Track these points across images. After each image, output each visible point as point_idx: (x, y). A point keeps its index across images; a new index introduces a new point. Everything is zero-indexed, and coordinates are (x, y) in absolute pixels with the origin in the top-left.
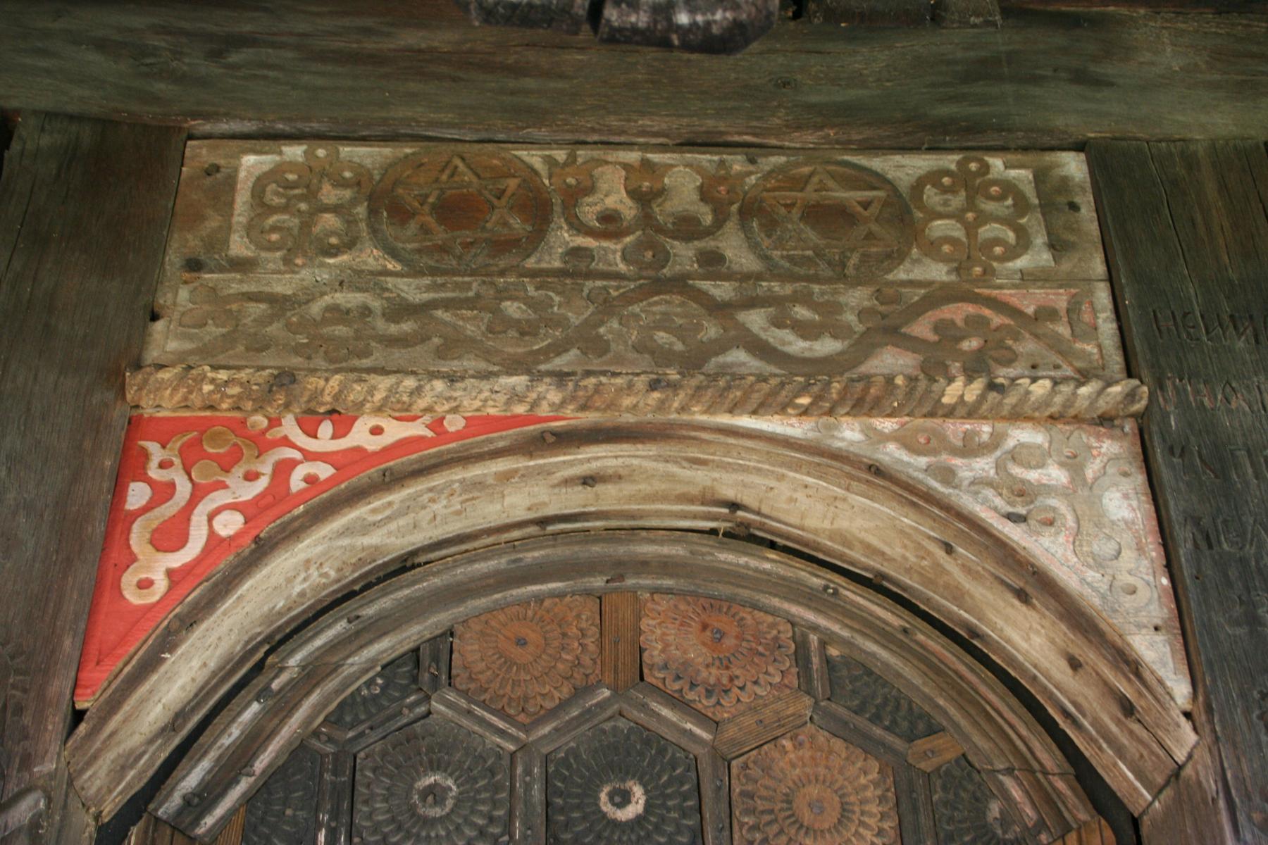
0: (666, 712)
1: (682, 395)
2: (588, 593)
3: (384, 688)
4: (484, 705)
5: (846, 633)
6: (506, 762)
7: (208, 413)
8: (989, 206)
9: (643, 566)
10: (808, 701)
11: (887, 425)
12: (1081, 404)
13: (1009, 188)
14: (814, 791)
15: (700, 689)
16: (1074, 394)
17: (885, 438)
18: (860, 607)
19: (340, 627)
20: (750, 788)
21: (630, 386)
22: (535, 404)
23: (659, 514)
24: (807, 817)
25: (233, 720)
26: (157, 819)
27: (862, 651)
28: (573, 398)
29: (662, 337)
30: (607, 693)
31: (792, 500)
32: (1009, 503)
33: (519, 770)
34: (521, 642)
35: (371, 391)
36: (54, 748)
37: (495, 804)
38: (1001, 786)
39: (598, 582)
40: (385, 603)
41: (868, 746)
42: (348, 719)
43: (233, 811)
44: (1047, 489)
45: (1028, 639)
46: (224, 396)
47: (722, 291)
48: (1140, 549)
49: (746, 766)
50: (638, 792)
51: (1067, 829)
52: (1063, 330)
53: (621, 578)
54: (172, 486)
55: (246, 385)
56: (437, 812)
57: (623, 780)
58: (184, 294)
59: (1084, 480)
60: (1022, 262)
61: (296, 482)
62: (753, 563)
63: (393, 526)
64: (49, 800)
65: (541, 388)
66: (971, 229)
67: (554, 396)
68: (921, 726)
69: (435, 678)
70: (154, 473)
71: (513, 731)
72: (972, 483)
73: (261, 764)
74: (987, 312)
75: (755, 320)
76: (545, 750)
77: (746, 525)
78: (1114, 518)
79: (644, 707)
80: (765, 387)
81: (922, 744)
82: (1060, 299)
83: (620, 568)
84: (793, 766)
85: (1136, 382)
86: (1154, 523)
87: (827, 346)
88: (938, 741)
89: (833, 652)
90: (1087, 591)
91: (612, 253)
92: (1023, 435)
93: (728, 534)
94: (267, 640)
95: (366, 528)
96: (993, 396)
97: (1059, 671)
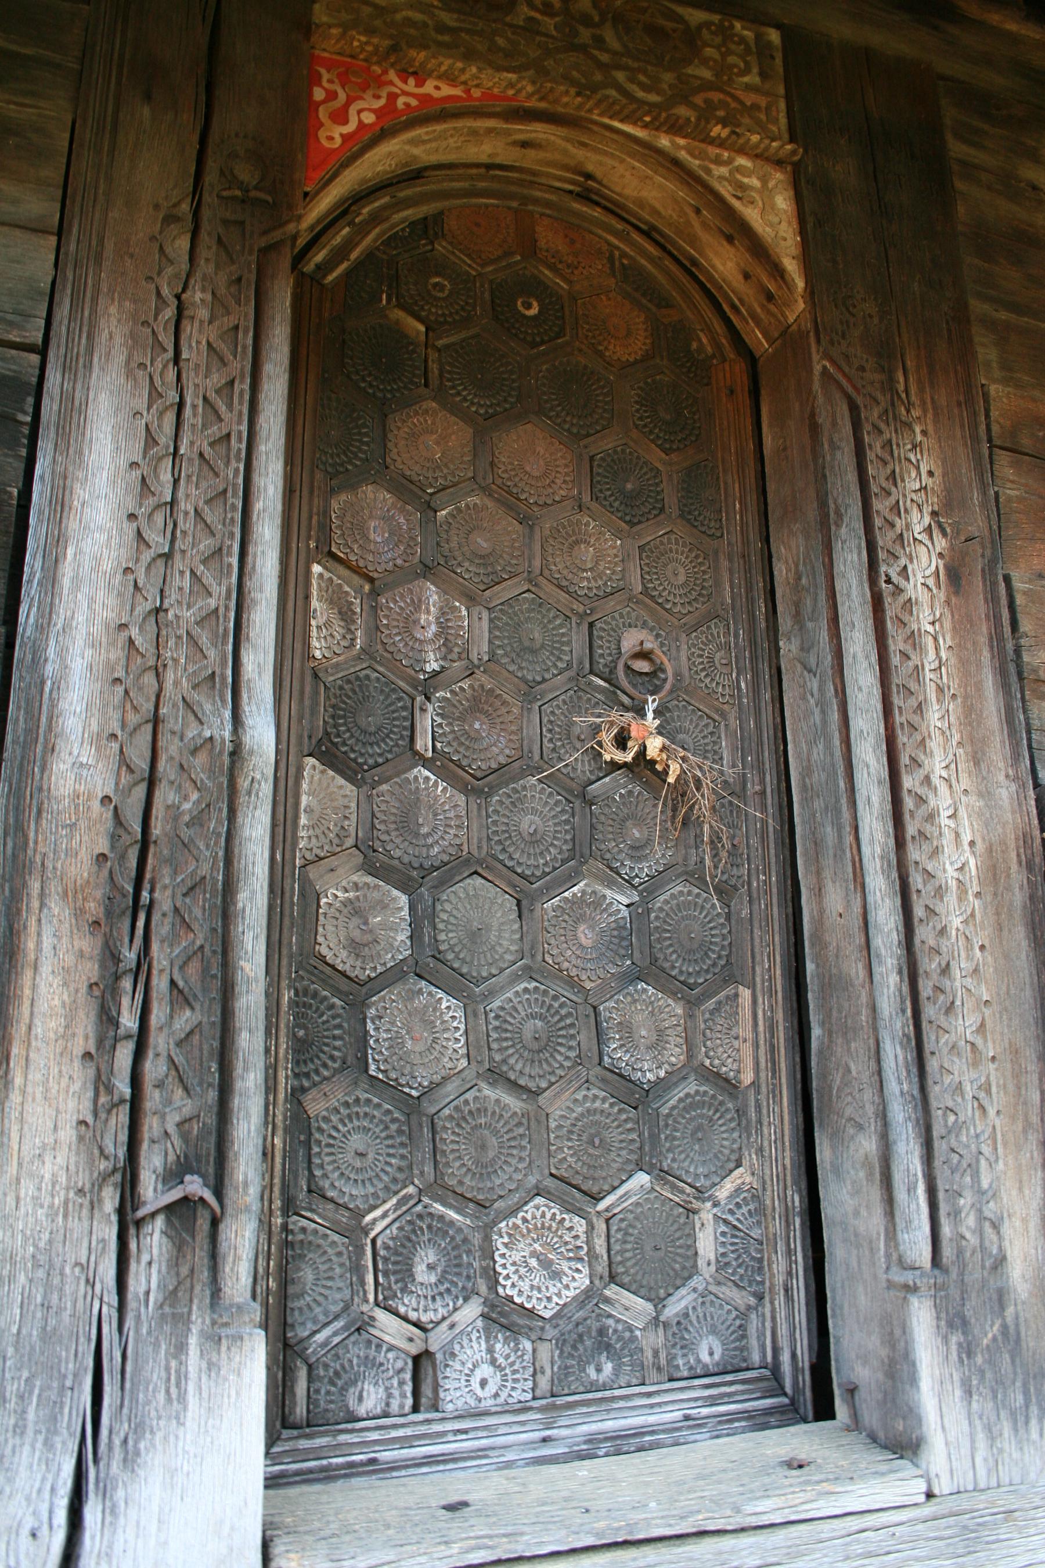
0: (547, 272)
2: (509, 208)
4: (460, 251)
8: (733, 47)
9: (536, 201)
11: (682, 142)
13: (743, 40)
17: (680, 148)
19: (387, 199)
22: (519, 91)
23: (548, 175)
26: (303, 274)
31: (622, 176)
34: (477, 225)
35: (440, 64)
39: (514, 204)
40: (408, 192)
44: (752, 188)
45: (724, 265)
47: (605, 58)
48: (789, 223)
50: (535, 304)
51: (724, 360)
52: (763, 117)
56: (441, 295)
60: (746, 79)
62: (589, 211)
65: (524, 83)
66: (724, 56)
69: (436, 234)
70: (325, 84)
73: (354, 256)
74: (729, 100)
75: (620, 76)
77: (589, 190)
79: (536, 268)
82: (763, 102)
83: (525, 200)
87: (653, 98)
89: (625, 262)
91: (549, 24)
92: (742, 161)
93: (578, 195)
96: (734, 137)
97: (736, 280)
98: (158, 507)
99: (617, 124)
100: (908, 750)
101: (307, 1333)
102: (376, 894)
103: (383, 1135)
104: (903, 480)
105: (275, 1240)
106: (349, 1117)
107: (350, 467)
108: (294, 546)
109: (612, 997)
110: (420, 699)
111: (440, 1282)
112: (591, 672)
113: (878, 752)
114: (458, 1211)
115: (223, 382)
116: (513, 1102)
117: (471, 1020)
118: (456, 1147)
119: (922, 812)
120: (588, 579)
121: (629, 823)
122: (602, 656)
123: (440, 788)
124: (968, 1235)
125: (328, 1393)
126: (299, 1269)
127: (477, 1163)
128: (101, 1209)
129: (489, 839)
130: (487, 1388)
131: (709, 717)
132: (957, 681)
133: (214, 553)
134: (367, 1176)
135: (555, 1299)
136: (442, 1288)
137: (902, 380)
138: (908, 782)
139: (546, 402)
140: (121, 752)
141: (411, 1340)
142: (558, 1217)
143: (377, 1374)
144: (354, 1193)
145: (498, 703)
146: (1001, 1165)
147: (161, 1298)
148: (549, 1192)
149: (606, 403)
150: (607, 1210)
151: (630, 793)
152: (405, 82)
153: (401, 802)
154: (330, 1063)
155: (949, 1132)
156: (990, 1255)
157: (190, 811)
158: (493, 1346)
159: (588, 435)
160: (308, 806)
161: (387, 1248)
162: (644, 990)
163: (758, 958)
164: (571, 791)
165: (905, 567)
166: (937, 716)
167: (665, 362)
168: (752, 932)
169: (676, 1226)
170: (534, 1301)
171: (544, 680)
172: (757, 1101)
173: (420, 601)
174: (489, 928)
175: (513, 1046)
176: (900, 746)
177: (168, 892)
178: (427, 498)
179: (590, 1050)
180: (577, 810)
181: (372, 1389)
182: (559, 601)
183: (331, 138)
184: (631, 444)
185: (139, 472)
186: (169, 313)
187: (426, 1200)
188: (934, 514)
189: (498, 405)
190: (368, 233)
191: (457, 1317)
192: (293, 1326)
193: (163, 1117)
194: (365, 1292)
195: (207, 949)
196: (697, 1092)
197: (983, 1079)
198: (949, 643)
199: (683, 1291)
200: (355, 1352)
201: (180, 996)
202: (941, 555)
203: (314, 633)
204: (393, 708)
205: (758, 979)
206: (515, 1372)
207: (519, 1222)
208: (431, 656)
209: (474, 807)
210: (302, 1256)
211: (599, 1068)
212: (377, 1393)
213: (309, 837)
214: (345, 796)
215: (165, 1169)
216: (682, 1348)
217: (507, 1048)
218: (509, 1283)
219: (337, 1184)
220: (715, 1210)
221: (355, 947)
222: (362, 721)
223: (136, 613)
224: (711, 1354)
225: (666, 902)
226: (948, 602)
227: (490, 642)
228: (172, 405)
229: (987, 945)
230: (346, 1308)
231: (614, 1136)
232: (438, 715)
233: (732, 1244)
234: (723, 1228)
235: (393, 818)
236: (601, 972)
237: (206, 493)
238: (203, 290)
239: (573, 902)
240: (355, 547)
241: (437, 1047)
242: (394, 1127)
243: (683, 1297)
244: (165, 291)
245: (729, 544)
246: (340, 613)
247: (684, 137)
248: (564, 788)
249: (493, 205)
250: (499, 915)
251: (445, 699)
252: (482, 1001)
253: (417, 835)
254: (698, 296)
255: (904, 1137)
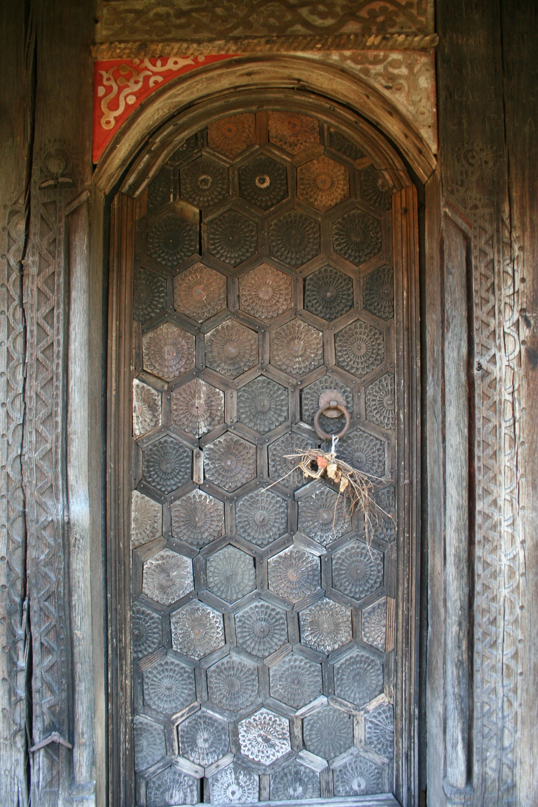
0: (277, 152)
1: (277, 46)
2: (251, 112)
3: (187, 148)
4: (219, 152)
5: (336, 124)
6: (226, 171)
7: (119, 59)
9: (269, 102)
10: (322, 147)
11: (348, 53)
12: (415, 44)
14: (323, 177)
15: (288, 144)
16: (413, 40)
18: (342, 115)
19: (171, 128)
20: (303, 176)
21: (259, 43)
22: (228, 51)
24: (320, 185)
25: (141, 160)
27: (341, 130)
28: (240, 48)
29: (272, 20)
30: (258, 147)
32: (387, 82)
33: (231, 173)
34: (230, 130)
35: (173, 49)
36: (89, 177)
37: (223, 184)
38: (383, 174)
39: (254, 108)
41: (341, 161)
42: (176, 158)
43: (144, 190)
44: (399, 76)
46: (124, 53)
48: (428, 98)
49: (302, 170)
50: (268, 179)
52: (414, 12)
53: (262, 106)
54: (111, 87)
55: (131, 49)
56: (206, 187)
57: (263, 175)
58: (105, 11)
59: (413, 73)
61: (151, 84)
62: (307, 99)
63: (185, 94)
64: (91, 192)
65: (229, 45)
67: (234, 48)
68: (359, 155)
69: (203, 144)
70: (105, 83)
71: (228, 160)
72: (375, 75)
73: (151, 174)
75: (304, 12)
76: (238, 166)
77: (304, 86)
78: (421, 87)
79: (269, 151)
80: (305, 41)
81: (359, 161)
83: (261, 103)
84: (317, 169)
85: (436, 34)
86: (435, 89)
87: (330, 22)
88: (364, 160)
89: (332, 130)
90: (408, 114)
92: (395, 56)
93: (298, 89)
94: (149, 134)
95: (176, 96)
96: (384, 42)
98: (16, 396)
99: (300, 54)
100: (482, 484)
101: (144, 768)
102: (173, 561)
103: (181, 679)
104: (500, 289)
105: (128, 726)
106: (163, 671)
107: (153, 315)
108: (122, 371)
109: (308, 607)
110: (196, 450)
111: (210, 747)
112: (301, 419)
113: (460, 489)
114: (220, 714)
115: (48, 311)
116: (250, 663)
117: (226, 622)
118: (218, 685)
119: (488, 524)
120: (299, 362)
121: (321, 511)
122: (307, 410)
123: (208, 500)
124: (490, 772)
125: (155, 794)
126: (140, 740)
127: (229, 692)
128: (15, 746)
129: (236, 526)
130: (235, 795)
131: (377, 439)
132: (526, 432)
133: (48, 416)
134: (172, 699)
135: (271, 757)
136: (212, 750)
137: (507, 209)
138: (479, 506)
139: (274, 247)
140: (8, 533)
141: (196, 772)
142: (273, 719)
143: (179, 786)
144: (165, 706)
145: (241, 448)
146: (519, 734)
147: (44, 784)
148: (269, 706)
149: (315, 239)
150: (302, 715)
151: (322, 493)
152: (155, 65)
153: (186, 509)
154: (152, 645)
155: (483, 716)
156: (506, 782)
157: (44, 559)
158: (238, 777)
159: (303, 264)
160: (135, 517)
161: (183, 731)
162: (327, 603)
163: (401, 581)
164: (286, 494)
165: (494, 355)
166: (507, 458)
167: (359, 199)
168: (398, 566)
169: (342, 723)
170: (260, 757)
171: (270, 430)
172: (395, 659)
173: (195, 392)
174: (236, 574)
175: (249, 635)
176: (477, 482)
177: (36, 601)
178: (199, 326)
179: (294, 635)
180: (289, 505)
181: (177, 793)
182: (281, 378)
183: (108, 122)
184: (332, 264)
185: (5, 378)
186: (15, 275)
187: (203, 709)
188: (522, 310)
189: (243, 255)
190: (160, 155)
191: (220, 762)
192: (138, 765)
193: (41, 706)
194: (173, 750)
195: (57, 626)
196: (357, 656)
197: (512, 686)
198: (523, 405)
199: (344, 755)
200: (168, 776)
201: (46, 650)
202: (523, 342)
203: (135, 421)
204: (181, 457)
205: (400, 594)
206: (249, 789)
207: (252, 721)
208: (202, 424)
209: (228, 508)
210: (141, 735)
211: (299, 644)
212: (179, 795)
213: (137, 534)
214: (155, 510)
215: (44, 728)
216: (342, 782)
217: (245, 636)
218: (246, 749)
219: (156, 703)
220: (366, 715)
221: (163, 589)
222: (164, 467)
223: (9, 459)
224: (359, 786)
225: (342, 554)
226: (526, 375)
227: (238, 411)
228: (20, 333)
229: (526, 605)
230: (163, 758)
231: (306, 679)
232: (206, 458)
233: (375, 733)
234: (369, 725)
235: (182, 519)
236: (302, 595)
237: (41, 382)
238: (33, 255)
239: (285, 558)
240: (157, 365)
241: (208, 637)
242: (186, 675)
243: (344, 758)
244: (12, 262)
245: (397, 321)
246: (149, 406)
247: (349, 49)
248: (282, 493)
249: (240, 113)
250: (242, 566)
251: (210, 449)
252: (233, 612)
253: (195, 527)
254: (384, 145)
255: (452, 717)
